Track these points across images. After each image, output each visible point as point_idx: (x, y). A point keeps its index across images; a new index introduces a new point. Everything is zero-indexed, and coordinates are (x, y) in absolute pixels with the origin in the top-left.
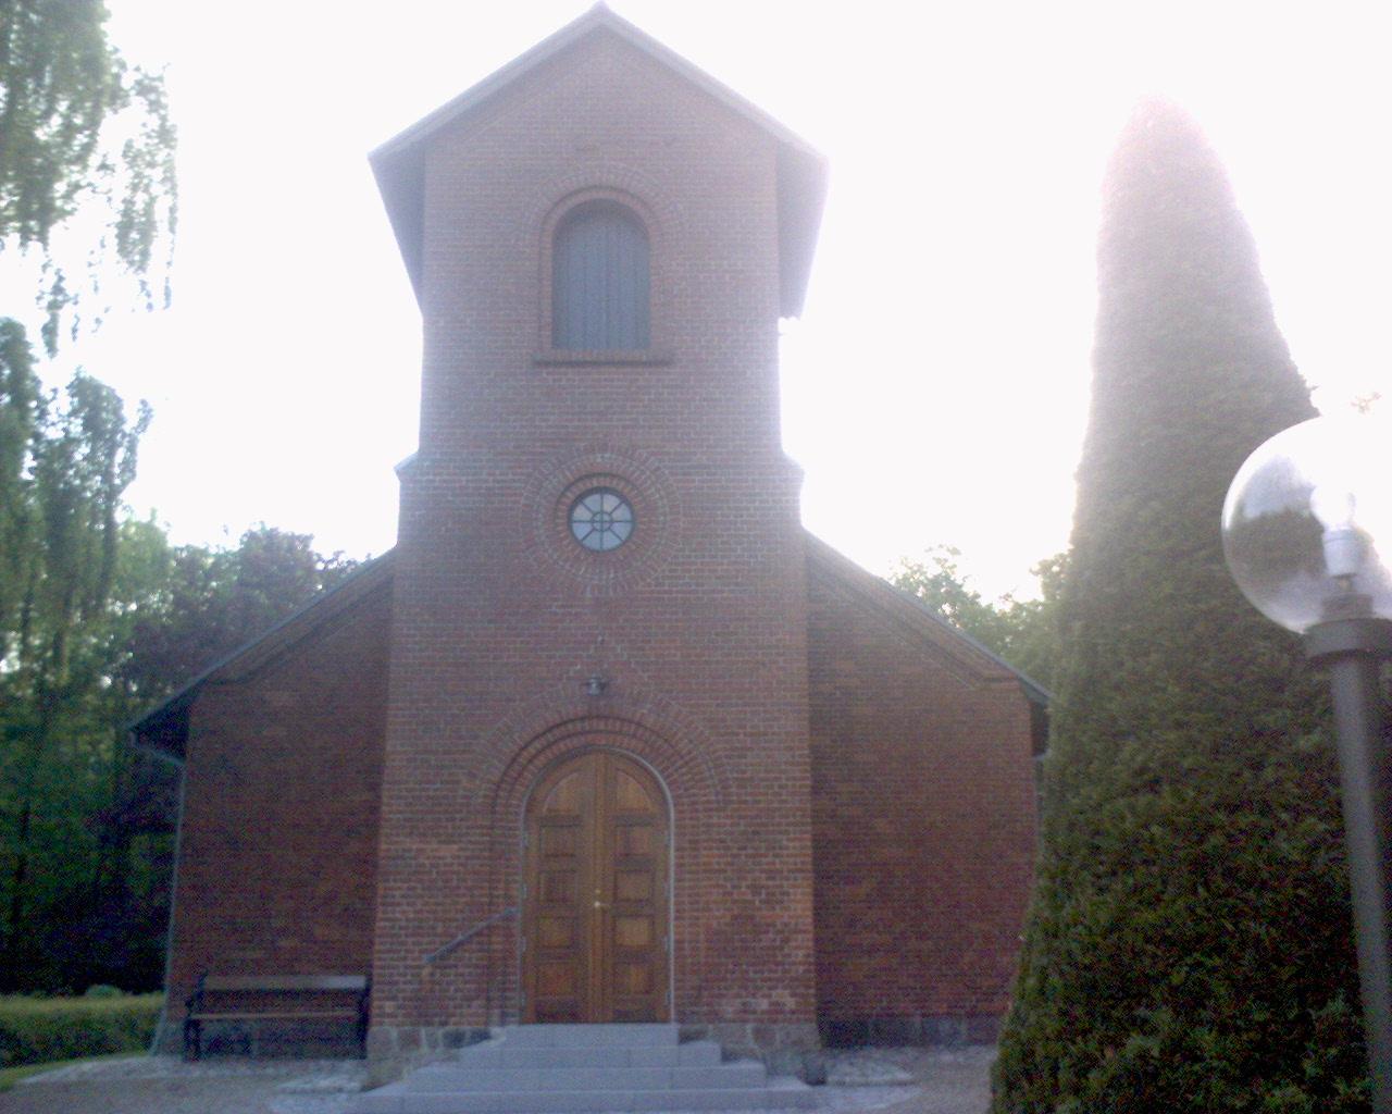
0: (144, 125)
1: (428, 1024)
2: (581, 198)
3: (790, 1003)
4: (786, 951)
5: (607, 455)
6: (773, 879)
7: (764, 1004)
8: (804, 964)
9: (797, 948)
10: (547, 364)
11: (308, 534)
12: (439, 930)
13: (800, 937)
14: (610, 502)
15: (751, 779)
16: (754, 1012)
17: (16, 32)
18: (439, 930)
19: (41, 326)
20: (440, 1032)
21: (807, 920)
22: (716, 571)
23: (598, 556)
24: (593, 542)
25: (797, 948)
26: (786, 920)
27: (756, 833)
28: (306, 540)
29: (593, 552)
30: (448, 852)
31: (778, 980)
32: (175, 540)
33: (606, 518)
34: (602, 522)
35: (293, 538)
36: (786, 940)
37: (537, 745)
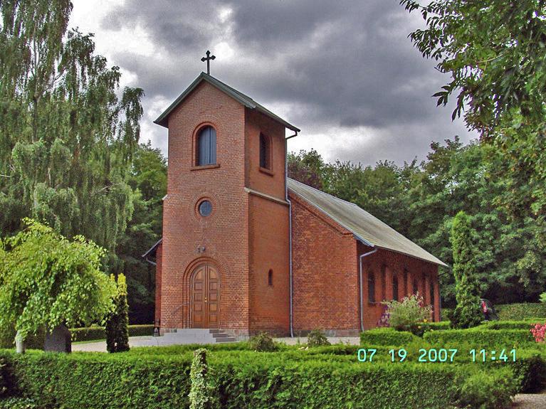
21: (247, 305)
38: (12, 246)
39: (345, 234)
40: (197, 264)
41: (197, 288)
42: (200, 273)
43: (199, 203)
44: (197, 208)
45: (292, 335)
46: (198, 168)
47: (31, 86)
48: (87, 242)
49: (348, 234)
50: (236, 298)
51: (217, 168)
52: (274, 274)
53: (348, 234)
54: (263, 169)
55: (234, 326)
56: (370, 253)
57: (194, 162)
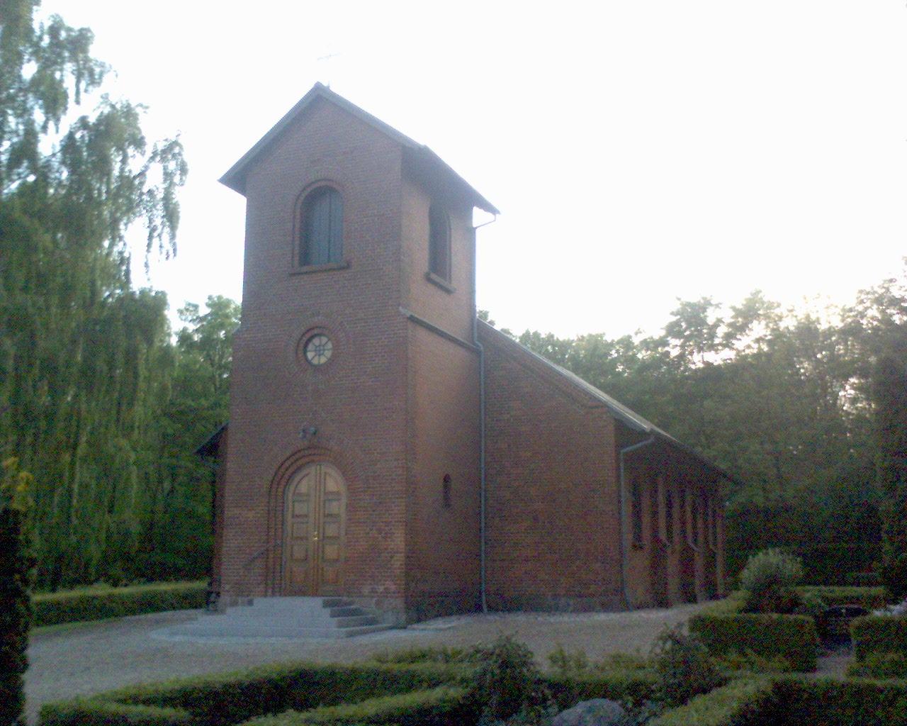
0: (145, 112)
1: (242, 596)
2: (314, 187)
3: (393, 588)
4: (392, 562)
5: (320, 318)
6: (388, 526)
7: (381, 589)
8: (399, 568)
9: (397, 560)
10: (294, 274)
11: (602, 333)
12: (247, 552)
13: (399, 555)
14: (316, 341)
15: (379, 475)
16: (377, 592)
17: (88, 168)
18: (247, 552)
19: (82, 115)
20: (246, 599)
21: (402, 545)
22: (366, 372)
23: (318, 369)
24: (315, 362)
25: (397, 560)
26: (392, 547)
27: (380, 503)
28: (601, 336)
29: (315, 366)
30: (251, 515)
31: (388, 576)
32: (830, 320)
33: (322, 352)
34: (320, 351)
35: (598, 335)
36: (392, 557)
37: (289, 462)
38: (796, 419)
39: (592, 408)
40: (299, 463)
41: (297, 512)
42: (304, 482)
43: (305, 339)
44: (302, 345)
45: (485, 607)
46: (305, 269)
47: (627, 345)
48: (797, 417)
49: (597, 407)
50: (380, 531)
51: (342, 268)
52: (454, 485)
53: (597, 407)
54: (433, 276)
55: (373, 591)
56: (639, 445)
57: (297, 258)
